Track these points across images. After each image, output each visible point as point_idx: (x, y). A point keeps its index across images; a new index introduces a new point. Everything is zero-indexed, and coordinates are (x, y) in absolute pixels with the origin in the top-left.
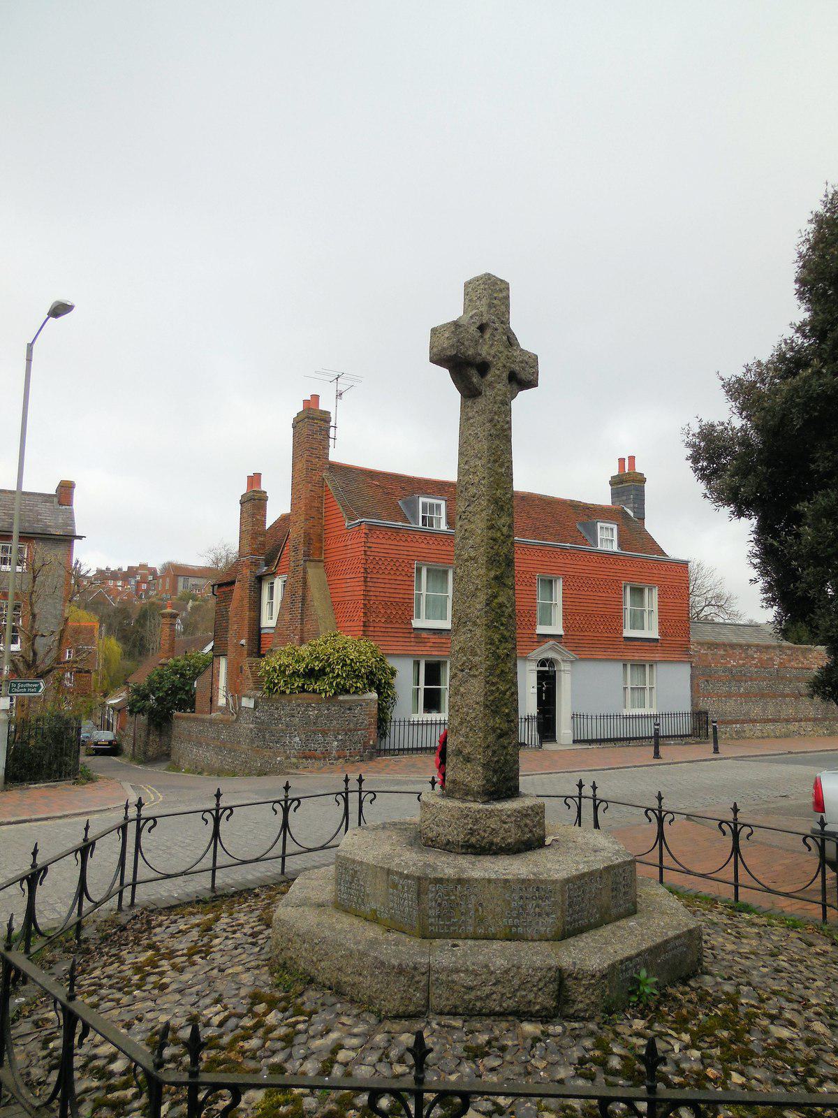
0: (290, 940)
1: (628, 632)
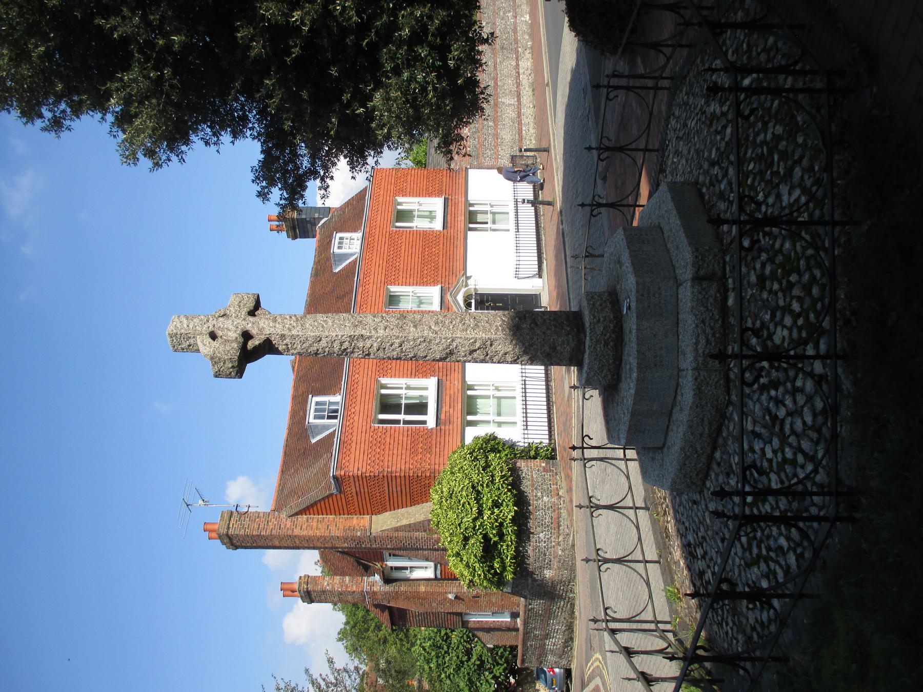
0: (685, 476)
1: (438, 225)
